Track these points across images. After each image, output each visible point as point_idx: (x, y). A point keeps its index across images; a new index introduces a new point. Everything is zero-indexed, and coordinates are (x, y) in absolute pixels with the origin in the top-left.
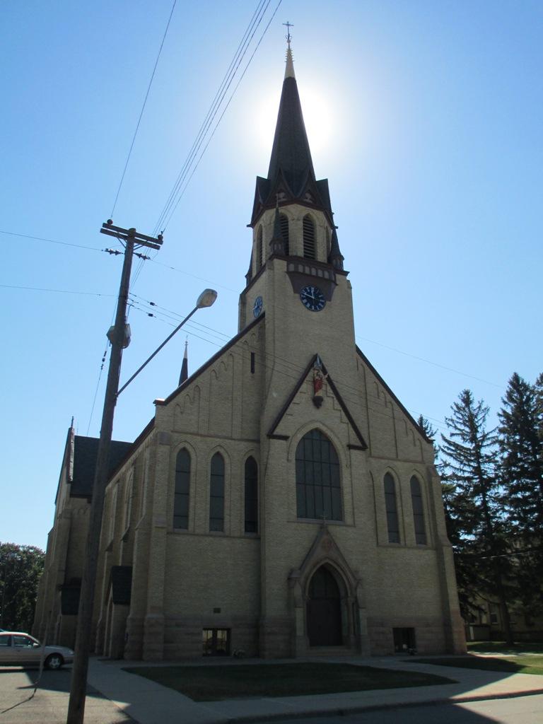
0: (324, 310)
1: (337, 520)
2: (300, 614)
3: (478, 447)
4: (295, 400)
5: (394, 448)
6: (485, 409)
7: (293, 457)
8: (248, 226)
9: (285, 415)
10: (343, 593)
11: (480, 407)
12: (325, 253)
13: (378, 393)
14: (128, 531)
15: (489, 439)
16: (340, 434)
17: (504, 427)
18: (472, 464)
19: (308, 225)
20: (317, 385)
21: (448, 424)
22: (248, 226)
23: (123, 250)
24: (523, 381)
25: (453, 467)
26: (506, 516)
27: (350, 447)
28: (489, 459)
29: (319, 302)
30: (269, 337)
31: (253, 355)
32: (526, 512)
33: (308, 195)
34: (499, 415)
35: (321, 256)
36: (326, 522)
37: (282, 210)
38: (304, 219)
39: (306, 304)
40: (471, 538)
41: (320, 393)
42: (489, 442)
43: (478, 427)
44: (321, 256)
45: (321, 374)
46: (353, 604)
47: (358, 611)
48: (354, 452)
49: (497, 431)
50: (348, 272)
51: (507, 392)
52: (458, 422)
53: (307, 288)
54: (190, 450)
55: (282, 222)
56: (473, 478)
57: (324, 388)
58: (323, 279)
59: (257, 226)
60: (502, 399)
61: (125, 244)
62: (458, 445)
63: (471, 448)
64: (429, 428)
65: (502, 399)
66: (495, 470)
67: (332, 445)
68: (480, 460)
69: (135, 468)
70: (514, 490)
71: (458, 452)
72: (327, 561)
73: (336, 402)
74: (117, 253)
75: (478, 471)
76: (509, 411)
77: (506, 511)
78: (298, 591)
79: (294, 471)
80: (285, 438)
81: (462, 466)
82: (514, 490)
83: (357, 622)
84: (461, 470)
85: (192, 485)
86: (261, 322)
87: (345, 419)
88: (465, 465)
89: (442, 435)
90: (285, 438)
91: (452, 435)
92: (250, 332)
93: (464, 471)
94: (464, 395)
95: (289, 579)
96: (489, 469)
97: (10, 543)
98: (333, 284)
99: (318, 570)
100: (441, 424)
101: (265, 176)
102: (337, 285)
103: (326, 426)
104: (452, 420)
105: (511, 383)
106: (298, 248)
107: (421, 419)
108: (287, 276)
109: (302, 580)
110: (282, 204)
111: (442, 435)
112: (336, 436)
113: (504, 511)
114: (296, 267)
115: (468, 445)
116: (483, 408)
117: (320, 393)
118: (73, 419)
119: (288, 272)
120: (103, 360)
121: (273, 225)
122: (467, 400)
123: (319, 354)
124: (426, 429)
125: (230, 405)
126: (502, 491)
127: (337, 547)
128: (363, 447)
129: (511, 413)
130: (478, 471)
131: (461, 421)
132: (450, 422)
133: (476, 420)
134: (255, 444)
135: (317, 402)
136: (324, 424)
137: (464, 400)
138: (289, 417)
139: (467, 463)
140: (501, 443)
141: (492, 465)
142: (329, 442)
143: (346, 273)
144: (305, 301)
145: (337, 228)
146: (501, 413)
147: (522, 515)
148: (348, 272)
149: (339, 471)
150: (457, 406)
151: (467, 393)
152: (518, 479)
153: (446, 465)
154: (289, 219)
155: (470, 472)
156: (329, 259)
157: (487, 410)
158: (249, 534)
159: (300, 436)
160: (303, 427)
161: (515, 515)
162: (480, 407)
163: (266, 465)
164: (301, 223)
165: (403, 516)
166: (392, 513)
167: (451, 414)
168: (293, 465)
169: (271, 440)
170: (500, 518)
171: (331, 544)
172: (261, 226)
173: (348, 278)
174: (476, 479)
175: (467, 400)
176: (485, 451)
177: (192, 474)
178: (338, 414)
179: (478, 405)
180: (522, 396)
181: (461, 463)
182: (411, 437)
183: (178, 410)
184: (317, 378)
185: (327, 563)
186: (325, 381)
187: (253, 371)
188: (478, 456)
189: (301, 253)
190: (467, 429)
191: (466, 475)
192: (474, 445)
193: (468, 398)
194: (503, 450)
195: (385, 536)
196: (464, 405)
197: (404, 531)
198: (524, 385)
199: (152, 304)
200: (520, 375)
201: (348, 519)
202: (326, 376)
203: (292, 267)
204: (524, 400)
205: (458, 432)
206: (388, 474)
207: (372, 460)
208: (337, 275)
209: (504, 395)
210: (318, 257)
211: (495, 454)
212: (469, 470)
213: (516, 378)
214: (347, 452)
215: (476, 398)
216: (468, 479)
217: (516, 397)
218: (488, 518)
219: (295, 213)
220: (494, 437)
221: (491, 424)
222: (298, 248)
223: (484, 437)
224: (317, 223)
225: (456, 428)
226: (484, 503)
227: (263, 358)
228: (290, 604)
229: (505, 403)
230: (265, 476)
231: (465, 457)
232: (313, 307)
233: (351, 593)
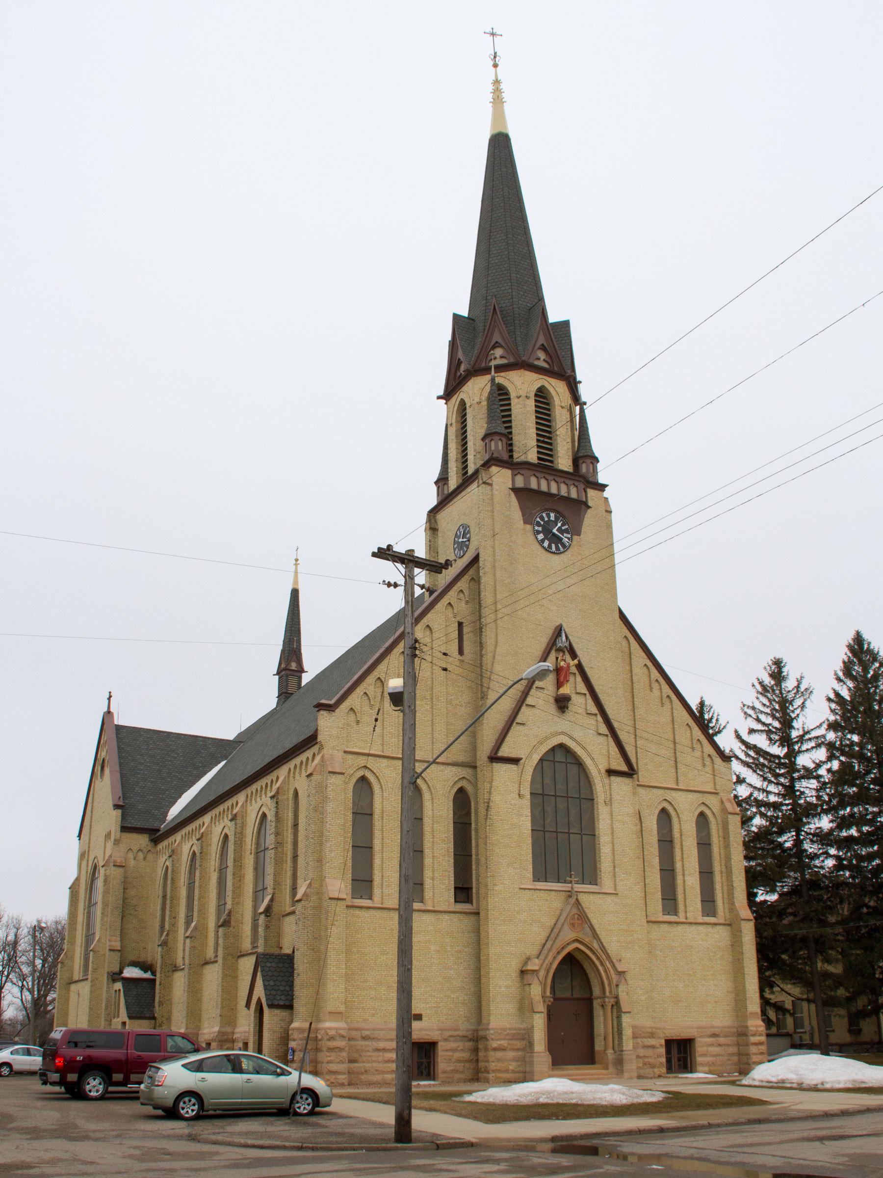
0: (569, 553)
1: (590, 883)
2: (539, 1023)
3: (792, 755)
4: (529, 700)
5: (674, 770)
6: (806, 689)
7: (526, 791)
8: (439, 398)
9: (515, 724)
10: (596, 991)
11: (798, 687)
12: (570, 454)
15: (810, 739)
16: (597, 754)
17: (836, 720)
18: (782, 780)
19: (542, 396)
21: (745, 713)
22: (439, 398)
23: (401, 581)
24: (869, 644)
25: (751, 785)
26: (830, 863)
27: (611, 772)
28: (809, 774)
29: (545, 522)
30: (487, 597)
31: (460, 625)
32: (861, 858)
33: (542, 355)
34: (829, 700)
35: (564, 462)
36: (579, 887)
37: (501, 379)
38: (536, 395)
39: (543, 541)
40: (773, 897)
41: (565, 690)
42: (813, 744)
43: (793, 719)
44: (564, 462)
45: (568, 657)
46: (612, 1006)
47: (619, 1017)
48: (615, 780)
49: (825, 726)
50: (606, 486)
51: (844, 662)
52: (762, 712)
53: (544, 515)
54: (372, 779)
55: (500, 397)
56: (782, 804)
57: (572, 678)
58: (567, 500)
59: (455, 400)
60: (836, 674)
61: (403, 571)
62: (761, 750)
63: (782, 755)
64: (714, 721)
65: (836, 674)
66: (817, 790)
67: (584, 770)
68: (796, 775)
69: (277, 803)
70: (844, 823)
71: (759, 761)
72: (576, 945)
73: (590, 701)
74: (396, 585)
75: (790, 791)
76: (845, 694)
77: (831, 856)
78: (536, 991)
79: (528, 812)
80: (515, 761)
81: (766, 783)
82: (844, 823)
83: (619, 1030)
84: (764, 791)
85: (377, 834)
86: (471, 572)
88: (770, 782)
89: (736, 731)
90: (515, 761)
91: (751, 731)
92: (456, 588)
93: (768, 793)
94: (773, 667)
95: (523, 972)
96: (808, 788)
98: (583, 507)
99: (564, 959)
100: (736, 715)
101: (465, 313)
102: (589, 507)
103: (575, 740)
104: (753, 708)
105: (850, 647)
106: (527, 446)
107: (702, 704)
108: (513, 495)
109: (542, 974)
110: (500, 368)
111: (736, 731)
112: (590, 756)
113: (828, 855)
114: (527, 481)
115: (777, 750)
116: (802, 688)
117: (565, 690)
118: (110, 697)
119: (515, 490)
120: (376, 720)
121: (485, 403)
122: (778, 672)
123: (565, 626)
124: (710, 720)
125: (428, 707)
126: (825, 823)
127: (591, 924)
128: (630, 772)
129: (848, 698)
130: (790, 791)
131: (768, 710)
132: (748, 710)
133: (791, 708)
134: (469, 771)
135: (562, 703)
136: (571, 738)
137: (772, 676)
138: (521, 728)
139: (773, 779)
140: (830, 746)
141: (814, 784)
142: (579, 764)
143: (602, 487)
144: (541, 536)
145: (580, 382)
146: (832, 696)
147: (854, 862)
148: (606, 486)
149: (593, 809)
151: (778, 663)
152: (853, 805)
153: (740, 781)
154: (513, 395)
155: (779, 794)
156: (576, 461)
157: (809, 691)
159: (536, 757)
160: (541, 743)
161: (845, 862)
162: (798, 687)
163: (488, 803)
164: (531, 404)
165: (684, 875)
166: (668, 873)
167: (751, 697)
168: (526, 802)
169: (494, 764)
170: (822, 867)
171: (581, 918)
172: (463, 403)
173: (606, 494)
174: (787, 805)
175: (778, 672)
176: (804, 761)
177: (376, 816)
178: (592, 721)
179: (795, 684)
180: (866, 670)
181: (765, 779)
182: (698, 753)
183: (352, 717)
184: (562, 664)
185: (577, 949)
186: (574, 669)
187: (461, 652)
188: (792, 767)
189: (532, 457)
190: (776, 724)
191: (772, 799)
192: (785, 750)
193: (780, 672)
194: (830, 758)
196: (773, 682)
197: (685, 900)
198: (870, 651)
199: (445, 654)
200: (866, 636)
201: (607, 883)
202: (576, 661)
203: (520, 482)
204: (869, 676)
205: (759, 727)
206: (664, 811)
207: (641, 791)
209: (839, 666)
210: (560, 461)
211: (818, 766)
212: (777, 791)
213: (858, 639)
214: (606, 781)
215: (792, 673)
216: (776, 806)
217: (857, 672)
218: (801, 867)
219: (522, 385)
220: (817, 738)
221: (815, 715)
222: (527, 446)
224: (557, 401)
225: (758, 720)
226: (798, 843)
227: (480, 631)
228: (525, 1007)
229: (839, 680)
230: (486, 819)
231: (770, 768)
232: (553, 546)
233: (610, 992)
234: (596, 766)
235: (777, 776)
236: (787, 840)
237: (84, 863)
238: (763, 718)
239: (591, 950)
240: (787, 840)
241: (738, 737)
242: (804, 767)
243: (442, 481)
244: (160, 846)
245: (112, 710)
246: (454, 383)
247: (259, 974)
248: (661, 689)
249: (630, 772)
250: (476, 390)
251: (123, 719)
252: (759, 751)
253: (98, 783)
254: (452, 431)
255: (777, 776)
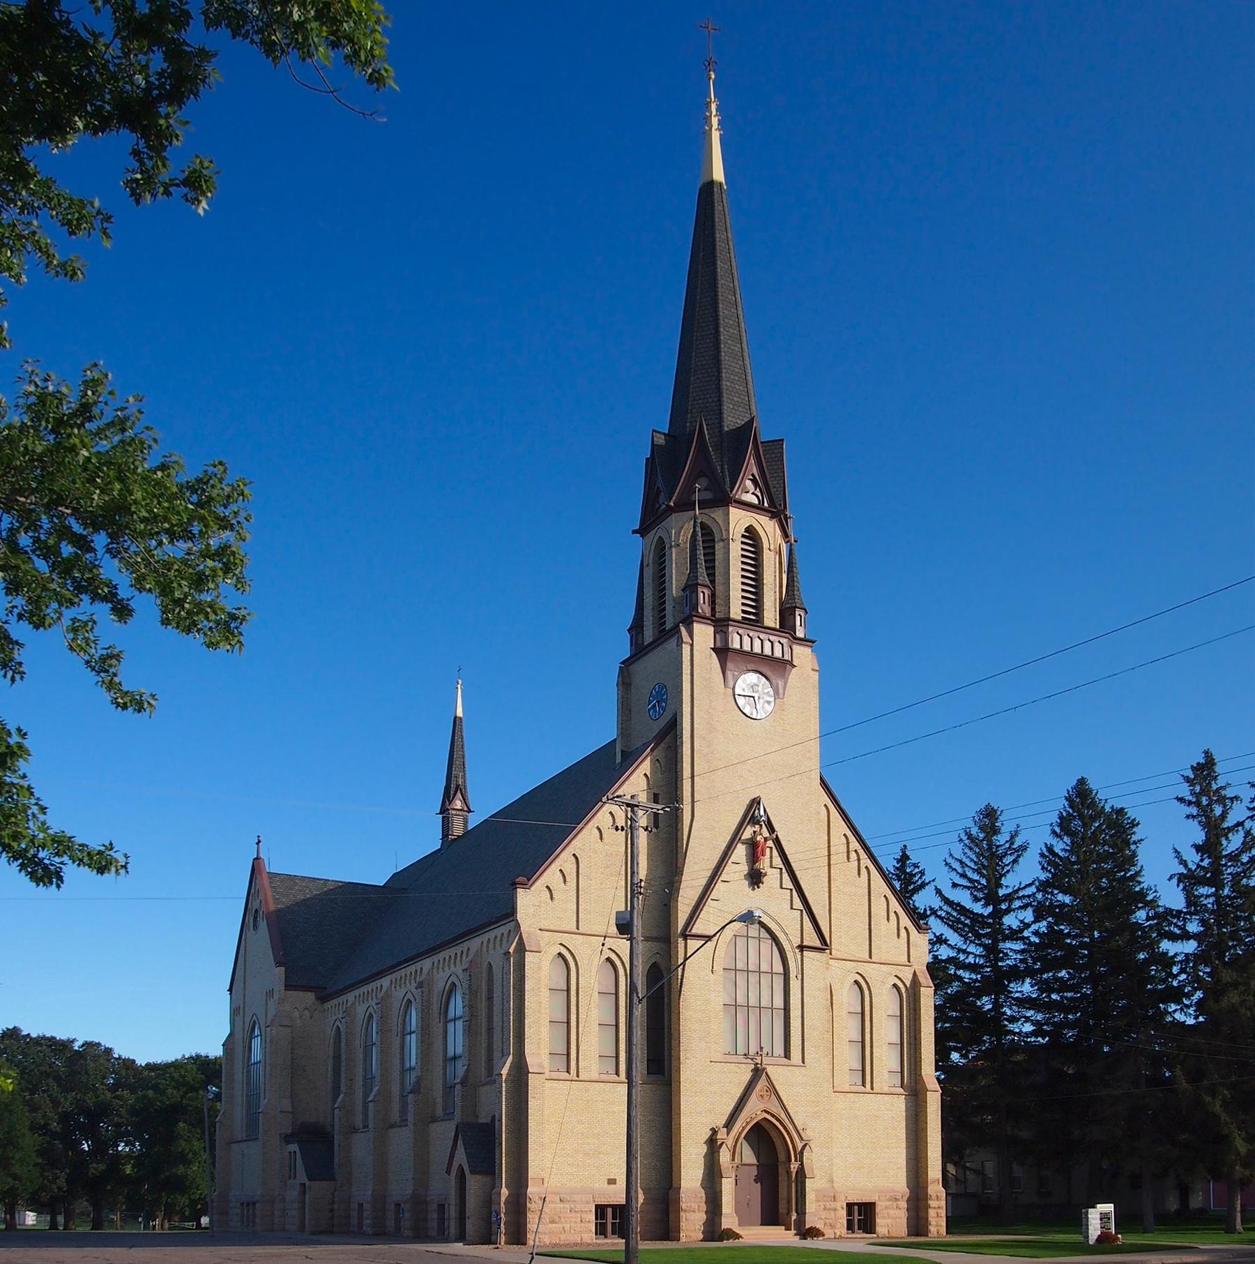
3: (998, 914)
8: (634, 532)
13: (848, 852)
14: (467, 1071)
20: (754, 851)
28: (1015, 935)
56: (982, 966)
59: (653, 536)
62: (963, 908)
71: (960, 919)
73: (785, 875)
75: (993, 952)
76: (1059, 847)
87: (798, 903)
91: (955, 885)
97: (106, 1042)
115: (978, 908)
122: (990, 817)
126: (1026, 988)
130: (993, 952)
135: (755, 878)
141: (1018, 946)
150: (970, 836)
157: (1023, 848)
158: (653, 1077)
175: (990, 817)
176: (1010, 921)
181: (966, 939)
191: (971, 959)
192: (990, 909)
195: (846, 1079)
200: (1093, 784)
205: (965, 882)
208: (794, 647)
213: (1082, 782)
215: (1006, 828)
221: (1025, 873)
223: (1009, 898)
225: (963, 876)
234: (790, 941)
235: (978, 936)
236: (986, 1003)
237: (239, 1019)
238: (970, 874)
239: (778, 1120)
240: (986, 1003)
241: (938, 892)
242: (1010, 928)
243: (636, 628)
244: (328, 1005)
245: (262, 856)
246: (651, 518)
247: (460, 1142)
248: (859, 860)
249: (824, 945)
250: (680, 530)
251: (275, 865)
252: (963, 910)
253: (250, 933)
254: (648, 573)
255: (978, 936)
